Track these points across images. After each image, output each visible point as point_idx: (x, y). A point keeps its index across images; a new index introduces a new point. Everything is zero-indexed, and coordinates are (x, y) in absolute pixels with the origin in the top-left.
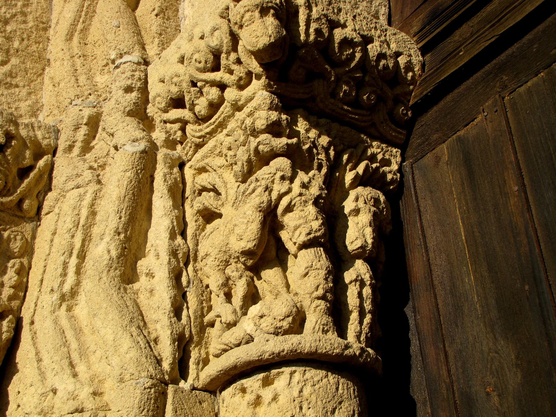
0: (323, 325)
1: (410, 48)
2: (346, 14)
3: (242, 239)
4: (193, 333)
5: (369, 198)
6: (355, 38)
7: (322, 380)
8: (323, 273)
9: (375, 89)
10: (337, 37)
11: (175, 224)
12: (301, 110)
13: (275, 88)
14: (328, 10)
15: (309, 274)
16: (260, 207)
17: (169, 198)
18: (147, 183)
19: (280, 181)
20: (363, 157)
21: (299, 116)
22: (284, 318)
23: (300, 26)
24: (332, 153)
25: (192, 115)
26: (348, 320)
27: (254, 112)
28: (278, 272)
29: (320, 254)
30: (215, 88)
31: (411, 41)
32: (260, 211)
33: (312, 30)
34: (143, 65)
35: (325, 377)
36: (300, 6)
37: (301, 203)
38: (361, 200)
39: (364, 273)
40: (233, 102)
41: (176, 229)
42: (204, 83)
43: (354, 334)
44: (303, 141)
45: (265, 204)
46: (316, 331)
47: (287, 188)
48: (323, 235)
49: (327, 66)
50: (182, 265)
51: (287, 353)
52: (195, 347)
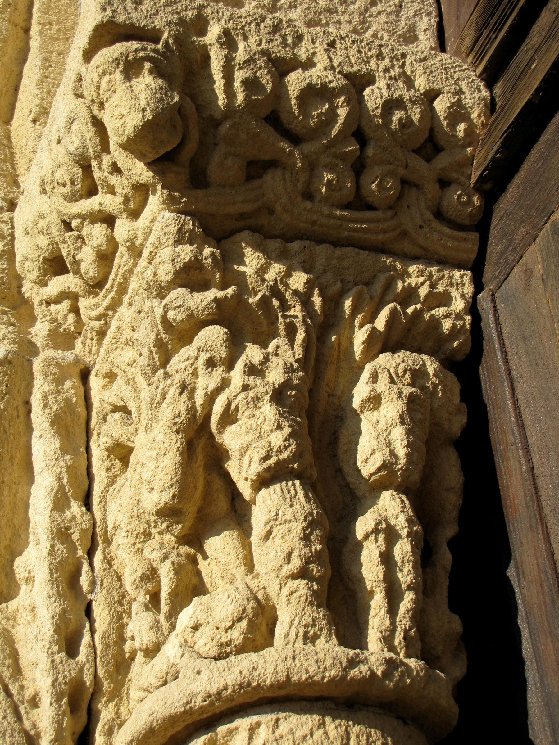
0: (306, 626)
1: (458, 79)
2: (313, 42)
3: (153, 489)
4: (101, 676)
5: (400, 370)
6: (331, 82)
7: (312, 735)
8: (298, 527)
9: (391, 167)
10: (293, 88)
11: (65, 481)
12: (246, 234)
13: (185, 202)
14: (270, 41)
15: (274, 534)
16: (175, 424)
17: (53, 436)
18: (18, 416)
19: (207, 369)
20: (387, 298)
21: (244, 245)
22: (233, 625)
23: (214, 82)
24: (317, 300)
25: (80, 282)
26: (368, 609)
27: (156, 253)
28: (229, 540)
29: (292, 491)
30: (99, 224)
31: (460, 66)
32: (178, 431)
33: (237, 84)
34: (8, 211)
35: (319, 728)
36: (210, 45)
37: (248, 404)
38: (383, 378)
39: (395, 514)
40: (128, 244)
41: (67, 489)
42: (79, 220)
43: (379, 635)
44: (253, 288)
45: (184, 416)
46: (292, 641)
47: (219, 379)
48: (297, 456)
49: (282, 145)
50: (80, 553)
51: (234, 691)
52: (109, 701)
